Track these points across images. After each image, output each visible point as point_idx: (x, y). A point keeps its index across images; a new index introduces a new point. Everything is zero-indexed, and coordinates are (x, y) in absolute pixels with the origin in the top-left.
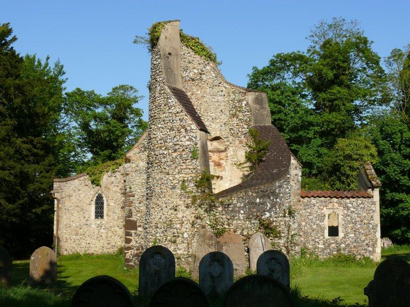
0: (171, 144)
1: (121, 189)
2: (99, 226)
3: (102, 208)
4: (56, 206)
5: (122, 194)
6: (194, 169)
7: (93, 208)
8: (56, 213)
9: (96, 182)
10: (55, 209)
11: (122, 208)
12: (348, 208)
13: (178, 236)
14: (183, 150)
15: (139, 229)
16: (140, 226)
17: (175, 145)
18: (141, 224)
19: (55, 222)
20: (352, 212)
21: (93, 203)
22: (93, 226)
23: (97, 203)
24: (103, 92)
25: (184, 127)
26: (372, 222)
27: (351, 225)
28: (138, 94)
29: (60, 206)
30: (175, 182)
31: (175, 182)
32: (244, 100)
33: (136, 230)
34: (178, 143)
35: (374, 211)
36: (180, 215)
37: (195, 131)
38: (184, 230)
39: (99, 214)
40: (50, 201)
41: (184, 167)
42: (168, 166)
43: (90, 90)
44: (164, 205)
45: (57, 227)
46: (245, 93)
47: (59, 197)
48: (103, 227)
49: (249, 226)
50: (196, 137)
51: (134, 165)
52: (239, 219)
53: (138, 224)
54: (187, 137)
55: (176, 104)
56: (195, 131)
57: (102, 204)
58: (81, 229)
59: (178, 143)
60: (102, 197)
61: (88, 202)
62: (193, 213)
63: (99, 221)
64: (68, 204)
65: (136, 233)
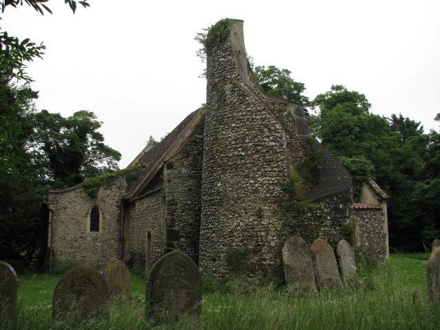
0: (251, 144)
1: (117, 202)
2: (95, 239)
3: (98, 220)
4: (50, 217)
5: (117, 207)
6: (280, 171)
7: (89, 220)
8: (50, 226)
9: (92, 196)
10: (50, 221)
11: (117, 221)
12: (364, 219)
13: (264, 245)
14: (267, 151)
15: (182, 239)
16: (182, 237)
17: (257, 145)
18: (183, 234)
19: (49, 235)
20: (367, 222)
21: (89, 216)
22: (89, 239)
23: (92, 216)
24: (67, 114)
25: (266, 126)
26: (382, 231)
27: (366, 235)
28: (99, 120)
29: (55, 218)
30: (257, 185)
31: (257, 185)
32: (285, 110)
33: (179, 240)
34: (260, 143)
35: (383, 222)
36: (265, 222)
37: (280, 131)
38: (270, 237)
39: (95, 227)
40: (45, 211)
41: (269, 169)
42: (247, 168)
43: (55, 112)
44: (243, 211)
45: (52, 240)
46: (286, 105)
47: (54, 209)
48: (99, 240)
49: (335, 232)
50: (281, 138)
51: (176, 172)
52: (326, 226)
53: (180, 234)
54: (271, 138)
55: (257, 102)
56: (280, 131)
57: (98, 216)
58: (76, 241)
59: (260, 143)
60: (98, 210)
61: (84, 214)
62: (280, 220)
63: (94, 234)
64: (63, 216)
65: (178, 244)
